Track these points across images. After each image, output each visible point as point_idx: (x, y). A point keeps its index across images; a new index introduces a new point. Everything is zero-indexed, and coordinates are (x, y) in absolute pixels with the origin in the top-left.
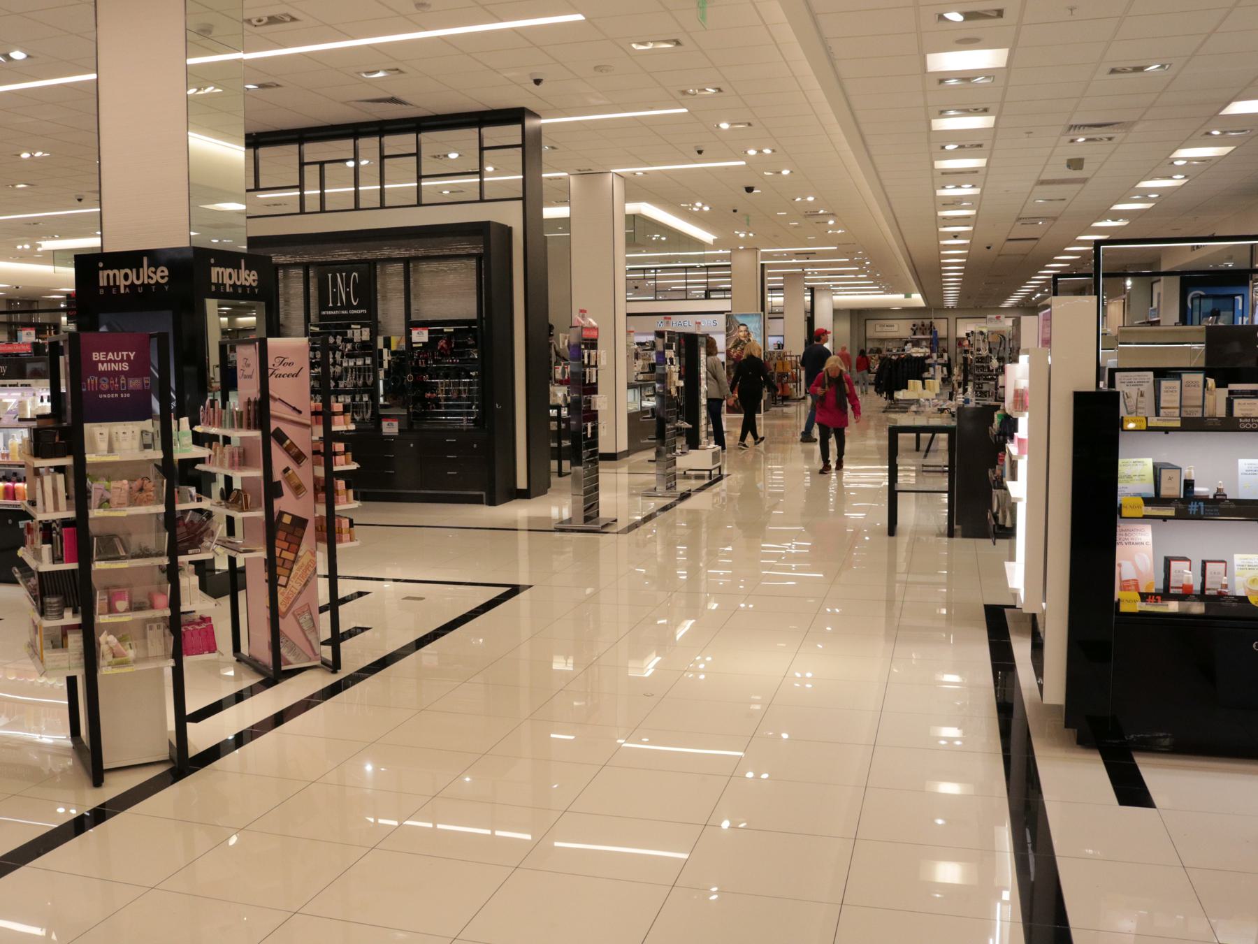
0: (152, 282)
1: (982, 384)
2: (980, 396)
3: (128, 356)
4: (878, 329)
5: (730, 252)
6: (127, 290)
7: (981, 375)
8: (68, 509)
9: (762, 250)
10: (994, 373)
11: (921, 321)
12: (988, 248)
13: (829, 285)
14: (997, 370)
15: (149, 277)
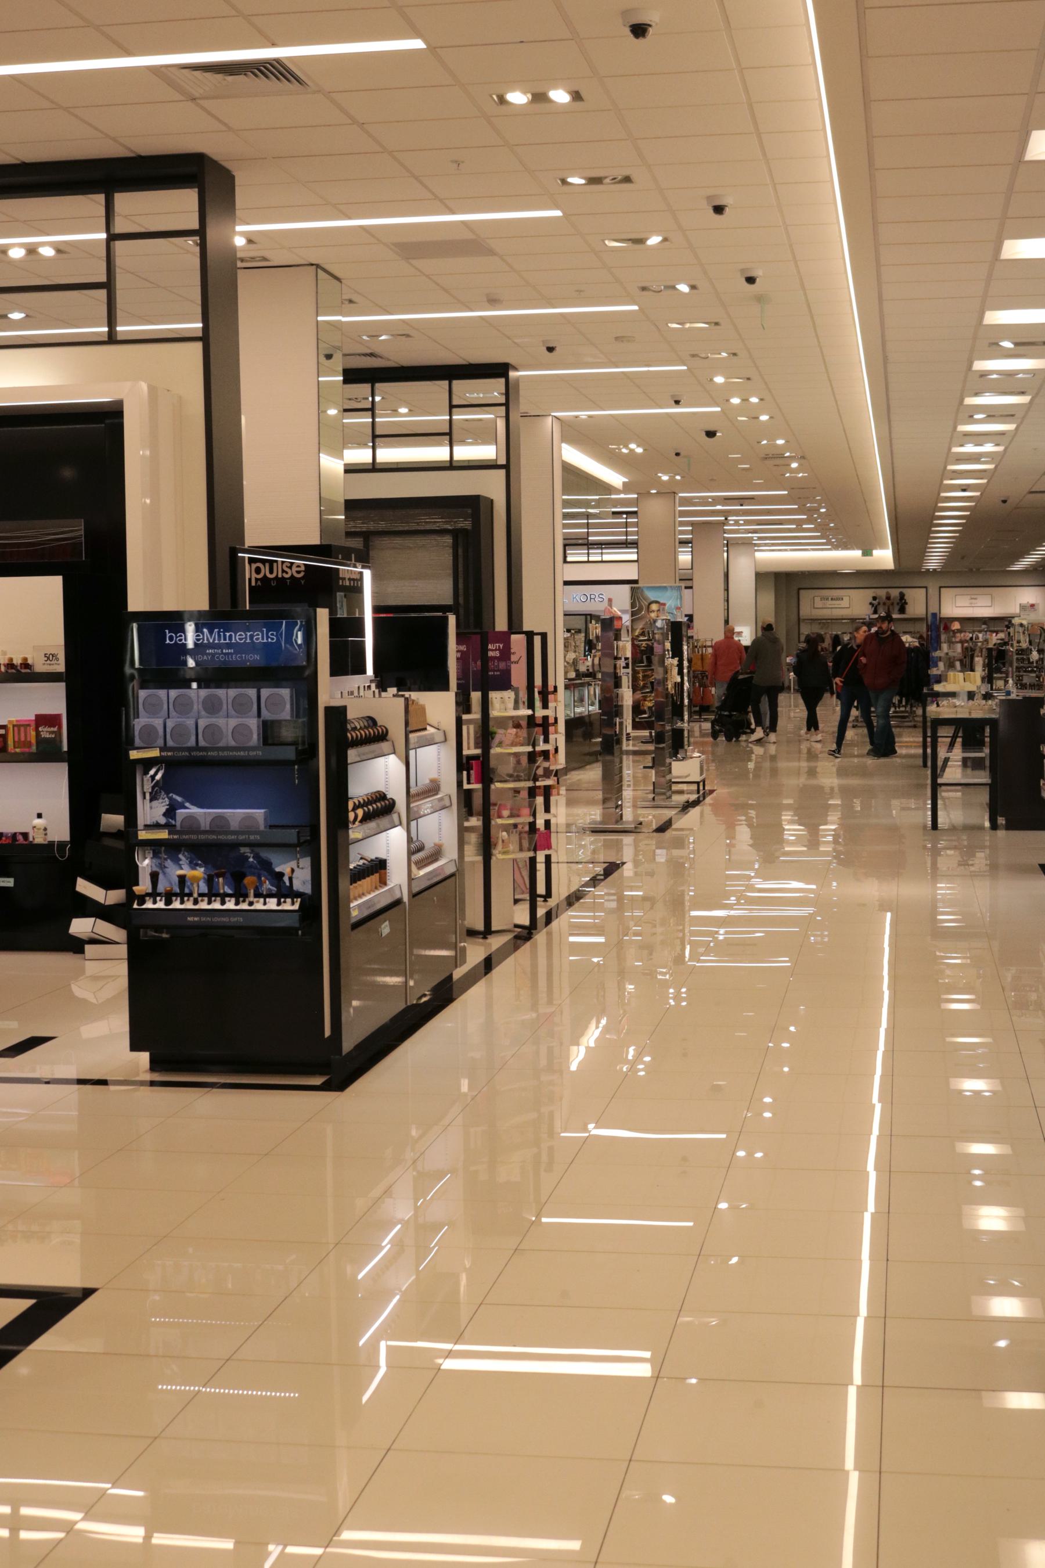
0: (286, 576)
1: (1022, 676)
2: (1021, 689)
3: (499, 646)
4: (818, 603)
5: (636, 496)
6: (259, 583)
7: (1021, 667)
8: (476, 747)
9: (680, 495)
10: (1035, 665)
11: (885, 591)
12: (1004, 502)
13: (752, 537)
14: (1037, 662)
15: (283, 571)
